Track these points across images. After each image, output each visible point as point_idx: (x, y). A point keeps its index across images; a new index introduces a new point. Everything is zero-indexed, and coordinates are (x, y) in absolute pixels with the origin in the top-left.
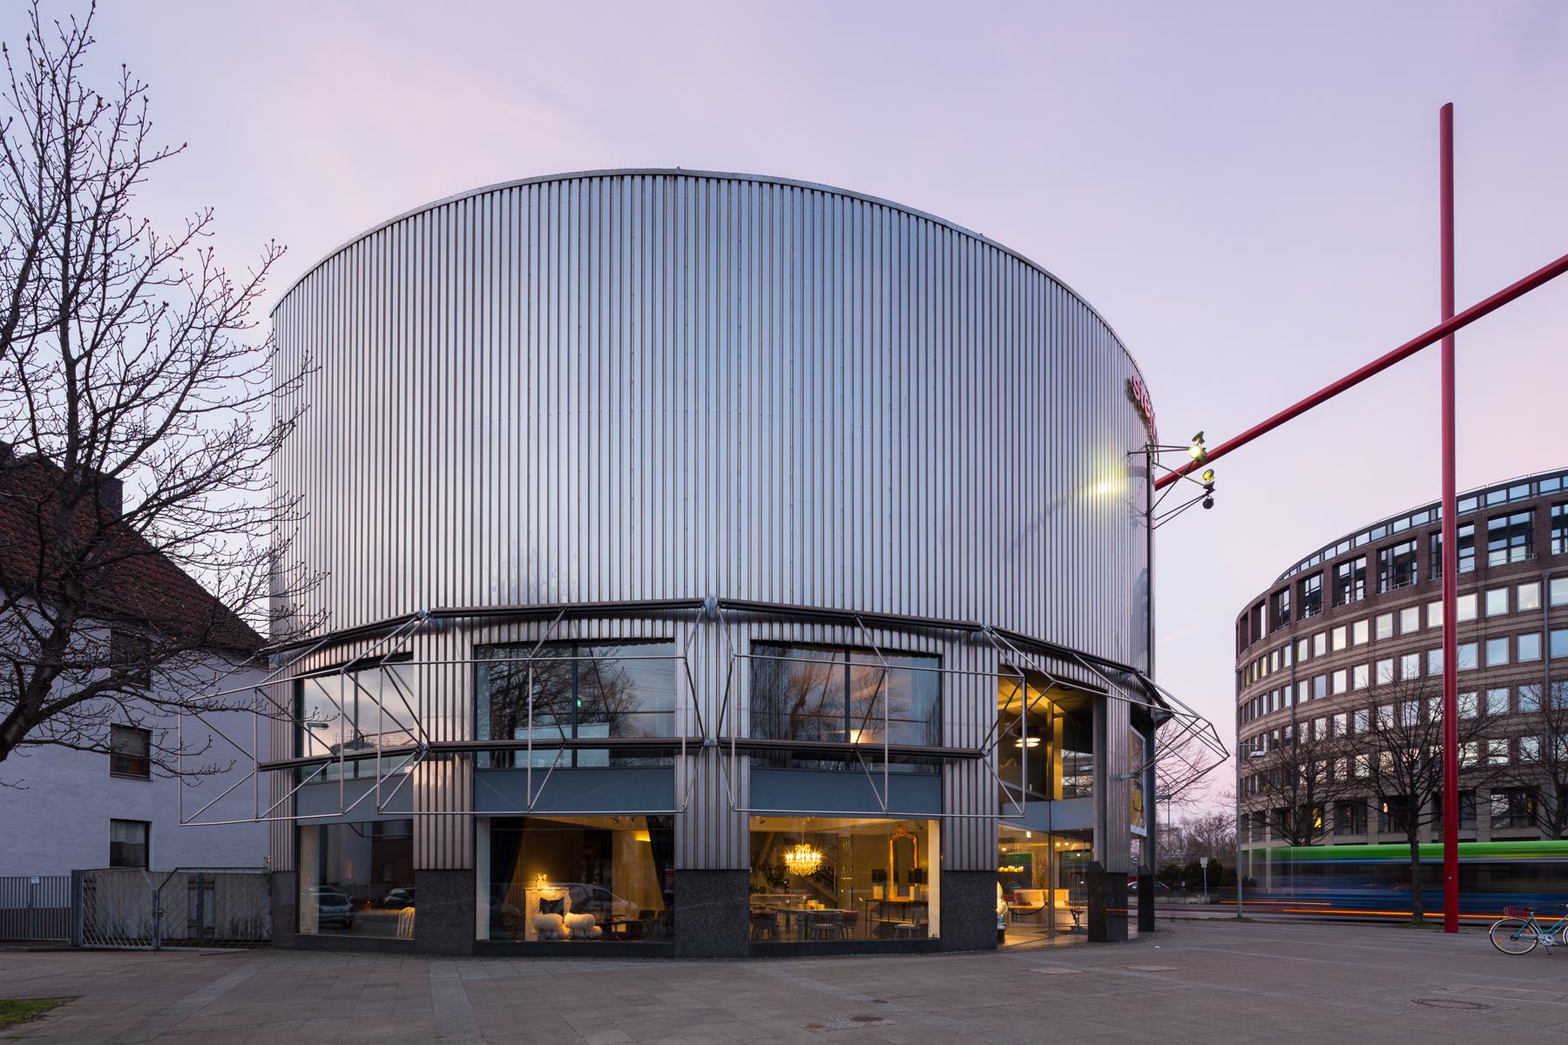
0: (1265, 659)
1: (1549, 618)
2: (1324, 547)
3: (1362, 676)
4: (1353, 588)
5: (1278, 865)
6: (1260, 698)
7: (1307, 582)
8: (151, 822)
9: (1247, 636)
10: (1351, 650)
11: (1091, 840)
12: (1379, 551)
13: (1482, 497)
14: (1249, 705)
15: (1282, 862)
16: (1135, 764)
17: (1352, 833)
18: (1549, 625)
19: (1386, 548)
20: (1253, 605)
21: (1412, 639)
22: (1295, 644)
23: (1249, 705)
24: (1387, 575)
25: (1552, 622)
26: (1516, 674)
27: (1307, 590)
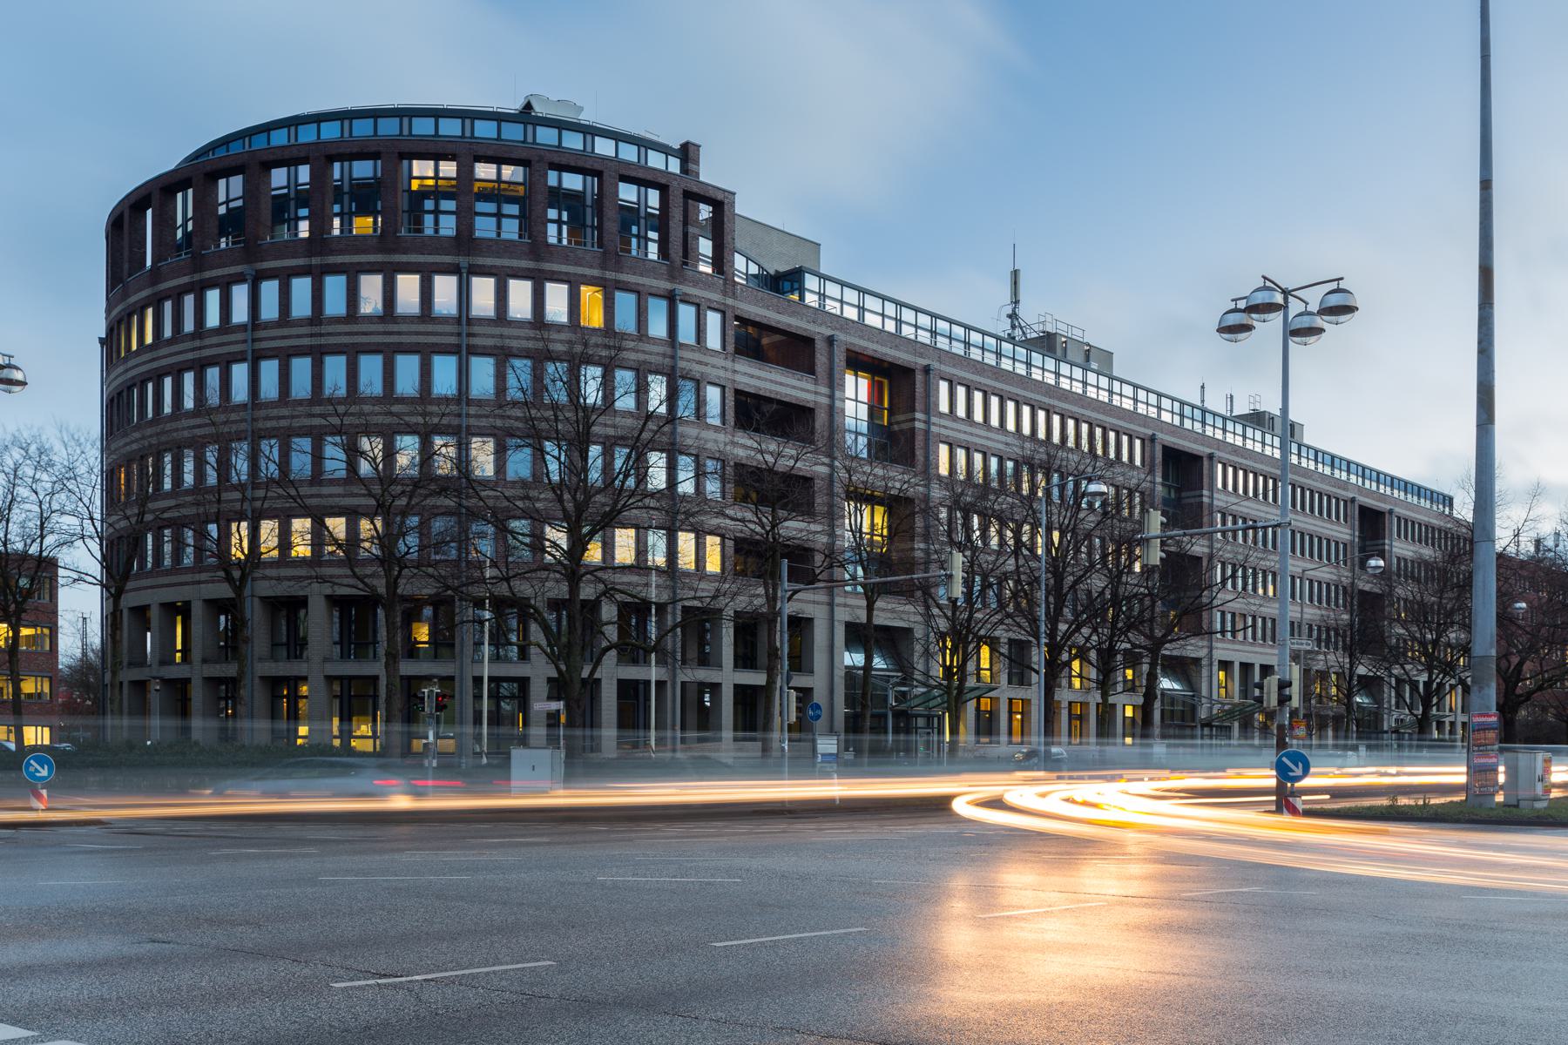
0: (150, 312)
1: (254, 340)
2: (296, 117)
3: (407, 370)
4: (292, 216)
5: (565, 773)
6: (143, 385)
7: (222, 183)
8: (529, 678)
9: (145, 253)
10: (320, 323)
11: (682, 738)
12: (331, 159)
13: (406, 120)
14: (125, 394)
15: (563, 765)
16: (706, 526)
17: (227, 659)
18: (253, 351)
19: (341, 158)
20: (132, 200)
21: (373, 328)
22: (199, 290)
23: (125, 394)
24: (342, 208)
25: (259, 345)
26: (960, 431)
27: (222, 198)
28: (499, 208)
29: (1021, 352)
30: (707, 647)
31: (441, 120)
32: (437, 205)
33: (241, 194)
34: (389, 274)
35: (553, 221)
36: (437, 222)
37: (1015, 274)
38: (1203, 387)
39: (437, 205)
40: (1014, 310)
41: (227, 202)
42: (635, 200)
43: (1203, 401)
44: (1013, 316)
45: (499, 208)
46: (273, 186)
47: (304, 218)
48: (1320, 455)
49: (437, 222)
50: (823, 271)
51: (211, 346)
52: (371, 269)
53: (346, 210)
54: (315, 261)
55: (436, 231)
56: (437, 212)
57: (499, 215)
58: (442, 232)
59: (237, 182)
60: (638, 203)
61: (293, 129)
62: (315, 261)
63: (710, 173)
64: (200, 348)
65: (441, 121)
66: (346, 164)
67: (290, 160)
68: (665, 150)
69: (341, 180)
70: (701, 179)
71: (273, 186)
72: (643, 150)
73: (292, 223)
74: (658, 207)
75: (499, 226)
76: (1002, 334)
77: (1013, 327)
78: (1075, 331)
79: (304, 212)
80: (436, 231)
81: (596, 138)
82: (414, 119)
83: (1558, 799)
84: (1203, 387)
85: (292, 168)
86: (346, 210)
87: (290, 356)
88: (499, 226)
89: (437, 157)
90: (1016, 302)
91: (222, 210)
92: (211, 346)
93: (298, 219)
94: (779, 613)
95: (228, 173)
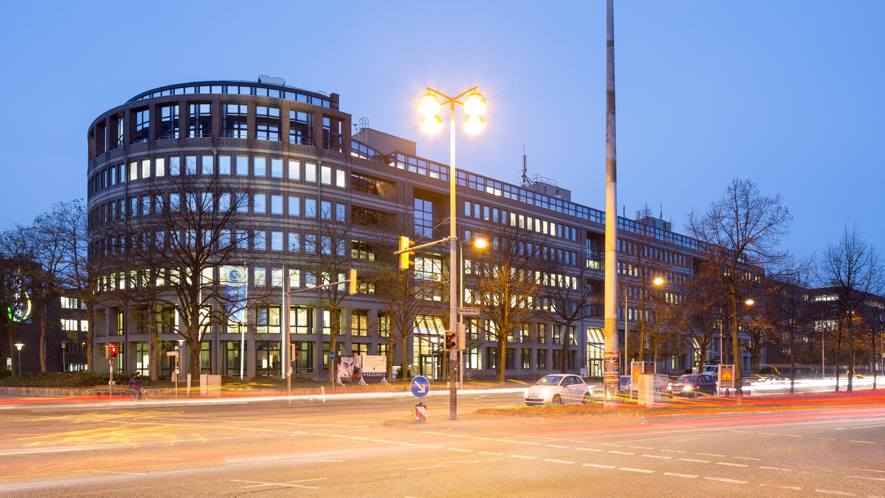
28: (268, 128)
29: (530, 195)
30: (340, 352)
31: (241, 87)
32: (239, 126)
33: (148, 120)
34: (199, 156)
35: (236, 129)
36: (239, 133)
37: (525, 156)
38: (624, 208)
39: (239, 126)
40: (524, 174)
41: (143, 124)
42: (306, 120)
43: (624, 214)
44: (524, 176)
45: (268, 128)
46: (163, 116)
47: (177, 131)
48: (675, 236)
49: (239, 133)
50: (418, 155)
51: (112, 193)
52: (175, 155)
53: (197, 127)
54: (151, 152)
55: (239, 137)
56: (239, 129)
57: (268, 131)
58: (242, 137)
59: (147, 113)
60: (307, 122)
61: (172, 90)
62: (151, 152)
63: (343, 108)
64: (108, 195)
65: (241, 88)
66: (197, 106)
67: (171, 103)
68: (322, 98)
69: (195, 114)
70: (340, 110)
71: (163, 116)
72: (309, 97)
73: (172, 133)
74: (328, 126)
75: (268, 135)
76: (519, 185)
77: (524, 181)
78: (551, 182)
79: (177, 129)
80: (239, 137)
81: (286, 93)
82: (228, 87)
83: (845, 365)
84: (624, 208)
85: (172, 107)
86: (197, 127)
87: (305, 198)
88: (268, 135)
89: (239, 104)
90: (525, 170)
91: (139, 128)
92: (112, 193)
93: (175, 131)
94: (333, 341)
95: (143, 109)
